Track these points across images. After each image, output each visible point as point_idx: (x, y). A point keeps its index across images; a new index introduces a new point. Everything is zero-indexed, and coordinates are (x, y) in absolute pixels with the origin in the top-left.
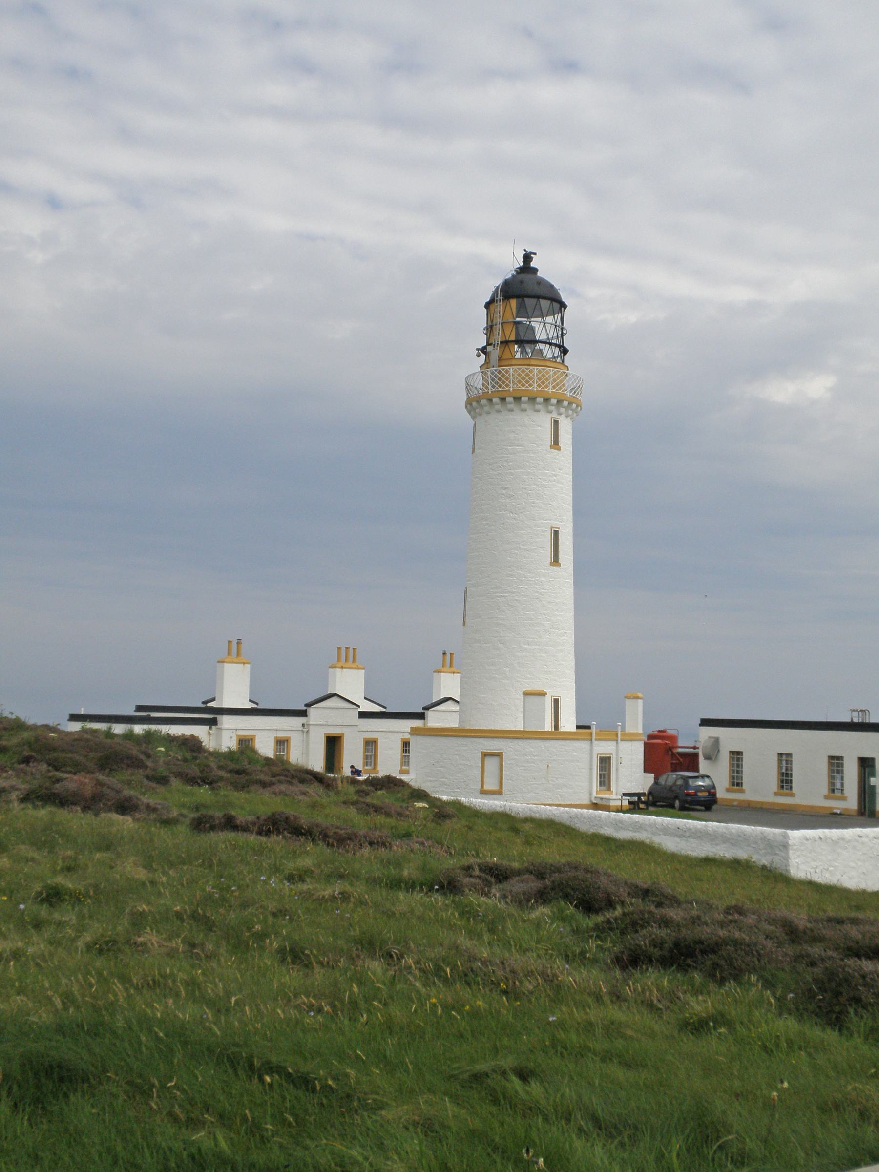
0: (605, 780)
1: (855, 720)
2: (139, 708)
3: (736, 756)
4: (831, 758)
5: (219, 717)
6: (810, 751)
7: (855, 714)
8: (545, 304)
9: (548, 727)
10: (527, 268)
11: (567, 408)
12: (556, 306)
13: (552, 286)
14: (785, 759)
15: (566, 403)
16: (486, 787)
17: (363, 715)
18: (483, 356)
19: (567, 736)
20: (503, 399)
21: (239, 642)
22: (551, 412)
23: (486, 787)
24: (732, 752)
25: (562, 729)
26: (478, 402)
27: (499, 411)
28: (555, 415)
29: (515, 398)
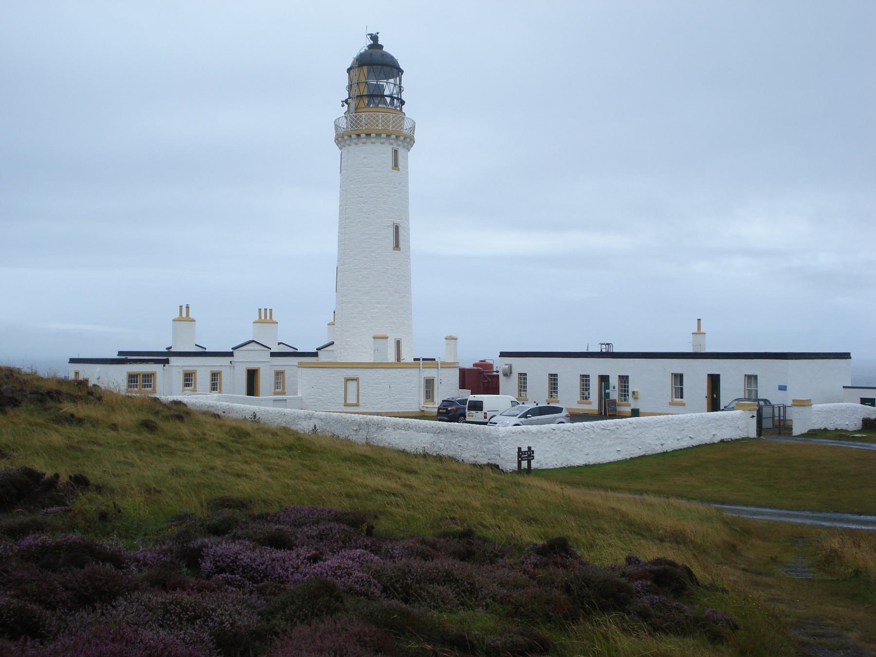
0: (429, 394)
1: (604, 351)
2: (120, 353)
3: (523, 376)
4: (583, 376)
6: (569, 373)
7: (604, 346)
9: (392, 358)
10: (375, 44)
12: (395, 71)
13: (392, 57)
14: (553, 379)
15: (402, 138)
16: (349, 402)
17: (273, 355)
18: (346, 106)
19: (408, 366)
20: (359, 135)
21: (188, 307)
22: (391, 144)
23: (349, 402)
24: (520, 374)
25: (407, 357)
26: (342, 137)
28: (395, 146)
29: (367, 135)
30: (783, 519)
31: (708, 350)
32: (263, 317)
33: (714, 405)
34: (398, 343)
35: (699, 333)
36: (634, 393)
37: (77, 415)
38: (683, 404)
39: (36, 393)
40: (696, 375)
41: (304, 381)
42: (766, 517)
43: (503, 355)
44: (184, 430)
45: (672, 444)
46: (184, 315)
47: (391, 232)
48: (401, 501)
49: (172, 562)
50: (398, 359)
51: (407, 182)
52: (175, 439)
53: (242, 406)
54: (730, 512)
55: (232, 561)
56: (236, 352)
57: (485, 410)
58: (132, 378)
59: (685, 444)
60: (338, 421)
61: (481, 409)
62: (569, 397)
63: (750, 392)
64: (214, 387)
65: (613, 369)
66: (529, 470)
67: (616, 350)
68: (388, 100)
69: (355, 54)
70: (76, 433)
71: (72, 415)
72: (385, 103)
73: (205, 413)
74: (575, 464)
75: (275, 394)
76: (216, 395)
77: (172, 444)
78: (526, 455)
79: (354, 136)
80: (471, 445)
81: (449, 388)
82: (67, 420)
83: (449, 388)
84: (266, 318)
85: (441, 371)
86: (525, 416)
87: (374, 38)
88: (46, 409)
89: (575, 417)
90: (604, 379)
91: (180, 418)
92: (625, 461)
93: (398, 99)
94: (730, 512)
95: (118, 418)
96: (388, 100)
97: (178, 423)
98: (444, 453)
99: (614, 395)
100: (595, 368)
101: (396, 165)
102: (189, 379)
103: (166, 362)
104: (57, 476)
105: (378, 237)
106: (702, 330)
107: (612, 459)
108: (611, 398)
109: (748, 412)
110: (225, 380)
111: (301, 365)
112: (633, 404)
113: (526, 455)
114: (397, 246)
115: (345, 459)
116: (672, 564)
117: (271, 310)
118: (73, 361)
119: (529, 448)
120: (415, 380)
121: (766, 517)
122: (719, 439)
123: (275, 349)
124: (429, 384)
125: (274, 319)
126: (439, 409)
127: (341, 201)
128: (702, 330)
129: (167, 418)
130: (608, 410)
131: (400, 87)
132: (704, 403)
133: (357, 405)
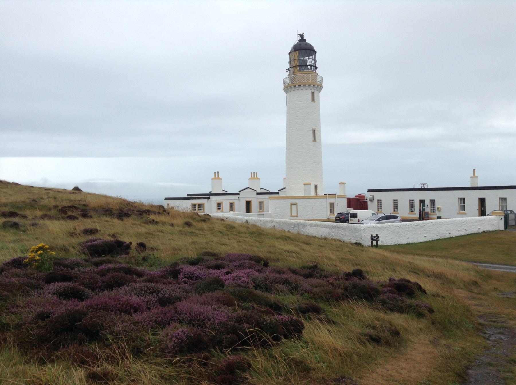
2: (188, 195)
3: (379, 201)
4: (411, 200)
5: (211, 197)
6: (404, 199)
9: (313, 194)
11: (317, 88)
14: (395, 202)
15: (316, 86)
16: (293, 215)
17: (258, 194)
18: (289, 71)
19: (321, 197)
20: (295, 86)
21: (218, 173)
23: (293, 215)
24: (378, 200)
25: (321, 193)
26: (287, 88)
27: (298, 90)
28: (313, 90)
30: (513, 271)
31: (479, 185)
33: (483, 213)
34: (316, 187)
35: (474, 176)
36: (438, 208)
37: (155, 220)
38: (466, 214)
39: (139, 211)
40: (472, 199)
41: (271, 205)
42: (502, 270)
43: (369, 191)
44: (205, 226)
45: (454, 234)
46: (217, 176)
47: (311, 133)
48: (295, 255)
49: (164, 275)
50: (316, 194)
51: (319, 108)
52: (199, 230)
53: (241, 217)
54: (481, 267)
55: (191, 275)
56: (240, 193)
57: (358, 218)
58: (194, 206)
59: (463, 233)
60: (285, 223)
61: (356, 217)
62: (404, 211)
63: (502, 207)
64: (231, 209)
65: (427, 196)
66: (377, 246)
67: (429, 187)
68: (309, 67)
69: (292, 45)
70: (152, 228)
71: (153, 220)
72: (308, 69)
73: (217, 219)
74: (402, 243)
75: (259, 212)
76: (232, 213)
77: (197, 232)
78: (375, 238)
79: (292, 87)
80: (348, 233)
81: (341, 207)
82: (150, 222)
83: (341, 207)
84: (254, 176)
85: (337, 199)
86: (378, 220)
87: (302, 36)
88: (142, 218)
89: (404, 220)
90: (422, 202)
91: (204, 221)
92: (429, 242)
93: (314, 66)
94: (481, 267)
95: (175, 222)
96: (309, 67)
97: (203, 223)
98: (335, 238)
99: (428, 209)
100: (417, 196)
101: (313, 100)
102: (219, 206)
103: (209, 198)
104: (131, 243)
105: (305, 136)
106: (476, 175)
107: (422, 241)
108: (426, 211)
109: (498, 217)
110: (236, 206)
111: (270, 198)
112: (438, 214)
113: (375, 238)
114: (315, 139)
115: (277, 238)
116: (409, 281)
118: (166, 199)
119: (377, 235)
121: (502, 270)
122: (482, 231)
123: (259, 191)
124: (332, 206)
126: (336, 217)
127: (287, 119)
128: (476, 175)
129: (198, 221)
130: (423, 216)
131: (315, 60)
132: (477, 212)
133: (297, 216)
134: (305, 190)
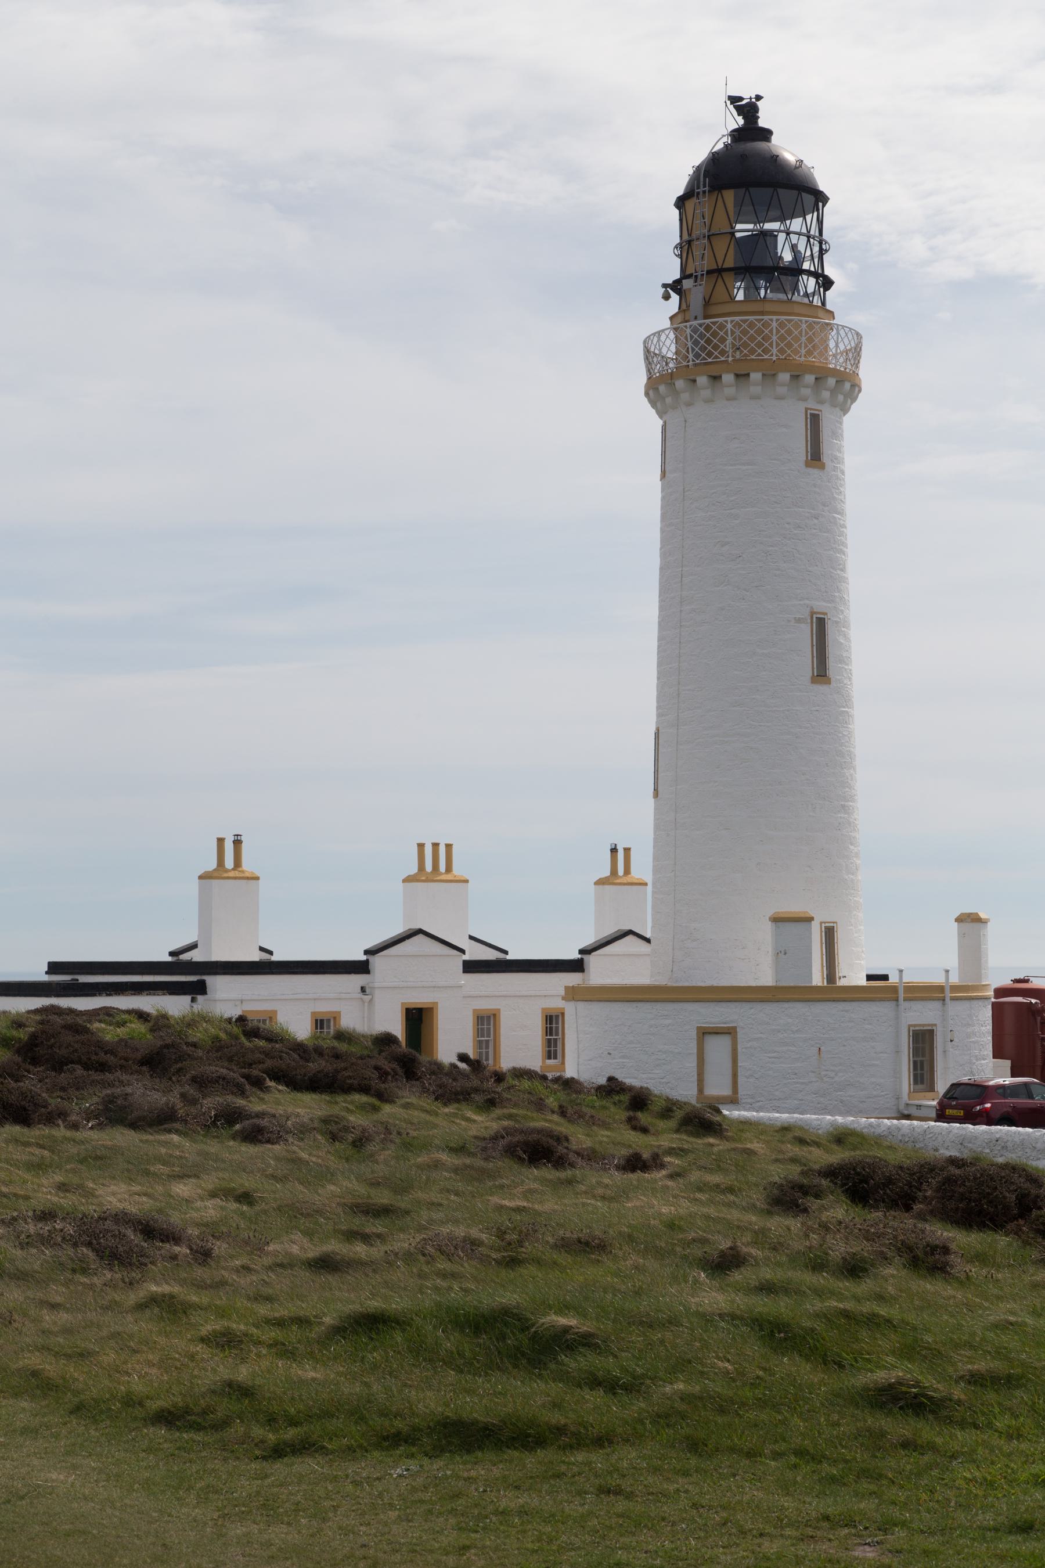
0: (923, 1072)
2: (54, 967)
5: (211, 981)
8: (786, 195)
9: (818, 979)
10: (750, 129)
12: (808, 199)
17: (472, 967)
18: (675, 298)
21: (237, 842)
28: (812, 404)
32: (429, 867)
46: (229, 863)
47: (805, 635)
50: (831, 976)
56: (377, 963)
69: (699, 155)
87: (748, 110)
105: (754, 643)
117: (449, 847)
120: (883, 1036)
124: (923, 1042)
125: (247, 865)
134: (780, 953)
